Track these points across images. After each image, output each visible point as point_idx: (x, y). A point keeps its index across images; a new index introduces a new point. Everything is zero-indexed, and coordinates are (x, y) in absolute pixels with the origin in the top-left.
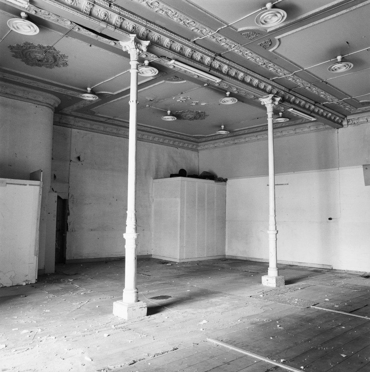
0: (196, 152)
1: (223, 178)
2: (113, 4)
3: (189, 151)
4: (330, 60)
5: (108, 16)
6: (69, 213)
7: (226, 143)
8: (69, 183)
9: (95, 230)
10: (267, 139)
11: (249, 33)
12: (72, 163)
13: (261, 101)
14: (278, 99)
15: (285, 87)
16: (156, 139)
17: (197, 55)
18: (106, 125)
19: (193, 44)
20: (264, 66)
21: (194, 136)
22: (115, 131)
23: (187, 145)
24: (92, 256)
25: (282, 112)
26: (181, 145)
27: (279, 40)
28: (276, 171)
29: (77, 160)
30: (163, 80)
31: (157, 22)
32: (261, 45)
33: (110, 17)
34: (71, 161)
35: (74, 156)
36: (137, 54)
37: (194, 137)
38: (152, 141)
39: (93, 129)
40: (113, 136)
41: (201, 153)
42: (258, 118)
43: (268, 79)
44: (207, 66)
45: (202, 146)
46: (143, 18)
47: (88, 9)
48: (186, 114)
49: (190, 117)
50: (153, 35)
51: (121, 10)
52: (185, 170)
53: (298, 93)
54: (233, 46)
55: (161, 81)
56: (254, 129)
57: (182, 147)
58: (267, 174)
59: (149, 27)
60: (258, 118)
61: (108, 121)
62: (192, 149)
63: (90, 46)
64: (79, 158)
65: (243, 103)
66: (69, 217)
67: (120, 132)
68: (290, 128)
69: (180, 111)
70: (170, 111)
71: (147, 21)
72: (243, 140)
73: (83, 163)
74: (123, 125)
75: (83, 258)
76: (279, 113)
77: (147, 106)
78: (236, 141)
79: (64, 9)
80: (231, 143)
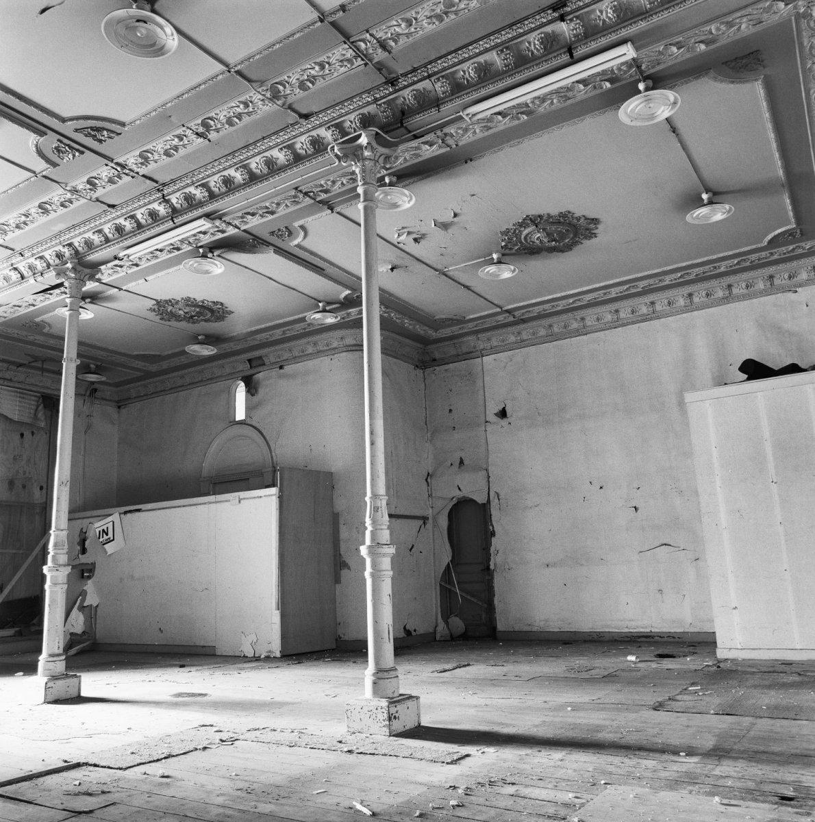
6: (494, 530)
9: (554, 565)
17: (599, 14)
24: (555, 626)
30: (661, 107)
34: (487, 422)
35: (493, 408)
40: (572, 339)
59: (503, 43)
64: (503, 414)
66: (494, 540)
73: (509, 420)
75: (535, 629)
79: (681, 9)
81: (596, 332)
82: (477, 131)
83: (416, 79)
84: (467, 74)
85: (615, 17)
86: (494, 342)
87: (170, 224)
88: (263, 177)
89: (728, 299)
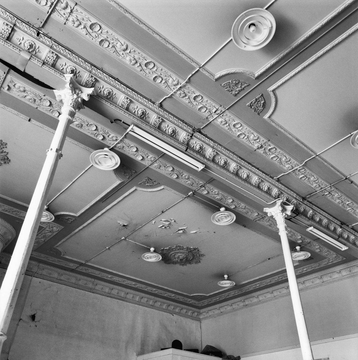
0: (198, 322)
1: (233, 356)
2: (42, 33)
3: (189, 319)
4: (350, 133)
5: (35, 48)
7: (234, 306)
8: (8, 353)
10: (289, 294)
11: (231, 81)
12: (21, 323)
13: (267, 211)
14: (290, 208)
15: (297, 194)
16: (144, 300)
18: (79, 276)
19: (160, 109)
20: (261, 151)
21: (192, 295)
22: (90, 285)
23: (185, 311)
25: (300, 246)
26: (177, 310)
27: (274, 91)
28: (312, 338)
29: (29, 320)
30: (134, 186)
31: (106, 68)
32: (251, 106)
33: (38, 50)
34: (21, 319)
36: (74, 100)
37: (193, 298)
38: (139, 303)
39: (61, 280)
41: (205, 323)
42: (269, 259)
43: (271, 177)
44: (182, 144)
45: (204, 314)
46: (86, 61)
47: (5, 32)
48: (173, 252)
49: (181, 257)
50: (102, 87)
51: (54, 43)
52: (182, 345)
53: (316, 206)
54: (214, 111)
55: (132, 187)
56: (268, 280)
57: (179, 314)
58: (296, 343)
60: (269, 259)
61: (81, 269)
62: (192, 318)
63: (29, 120)
64: (33, 317)
65: (245, 228)
67: (97, 288)
68: (314, 275)
69: (167, 247)
70: (154, 248)
71: (92, 65)
72: (255, 300)
73: (37, 324)
74: (99, 276)
76: (295, 248)
77: (122, 239)
78: (247, 303)
80: (241, 305)
81: (99, 294)
82: (28, 97)
83: (180, 125)
84: (196, 145)
85: (106, 95)
86: (44, 272)
87: (337, 237)
88: (240, 177)
89: (152, 307)
